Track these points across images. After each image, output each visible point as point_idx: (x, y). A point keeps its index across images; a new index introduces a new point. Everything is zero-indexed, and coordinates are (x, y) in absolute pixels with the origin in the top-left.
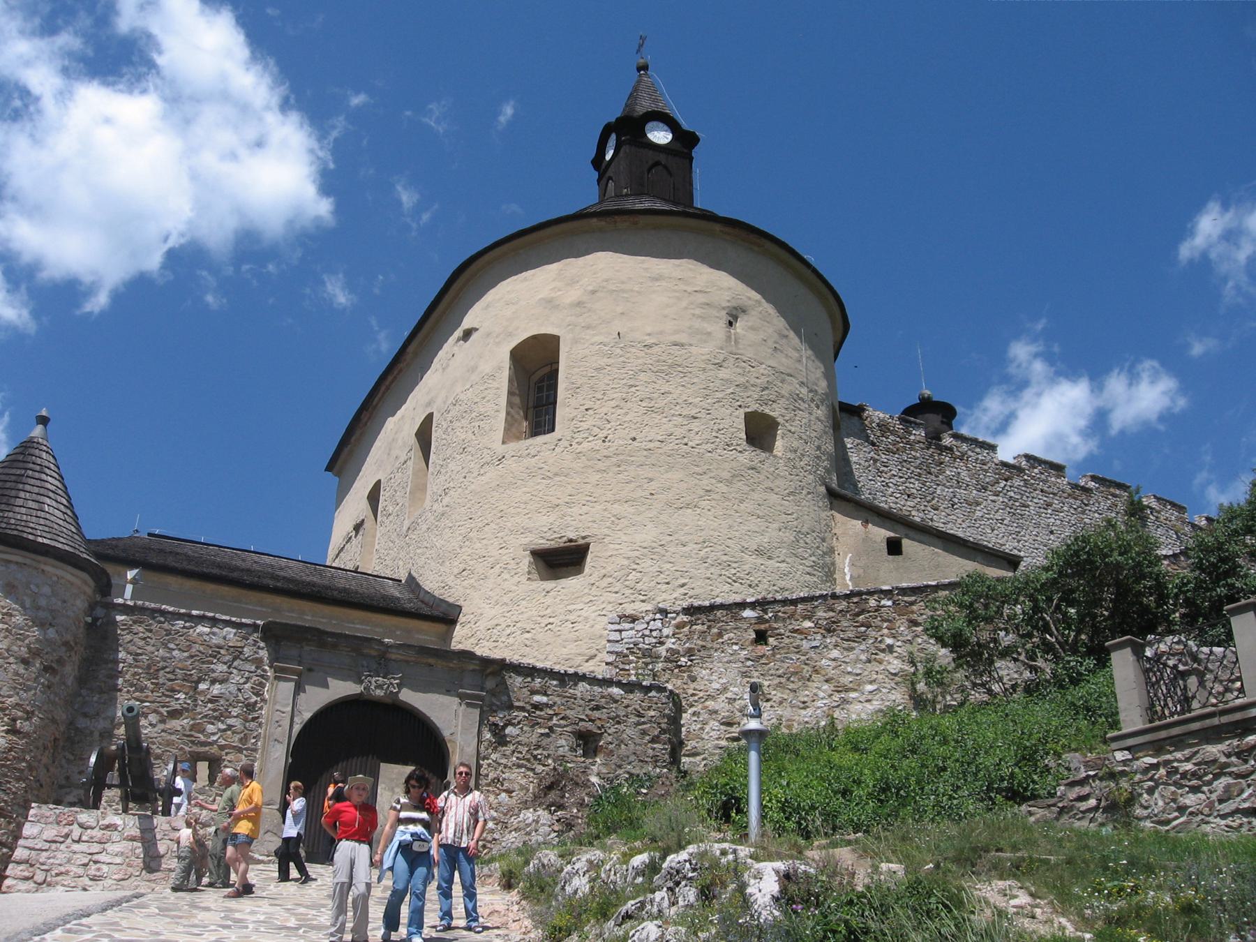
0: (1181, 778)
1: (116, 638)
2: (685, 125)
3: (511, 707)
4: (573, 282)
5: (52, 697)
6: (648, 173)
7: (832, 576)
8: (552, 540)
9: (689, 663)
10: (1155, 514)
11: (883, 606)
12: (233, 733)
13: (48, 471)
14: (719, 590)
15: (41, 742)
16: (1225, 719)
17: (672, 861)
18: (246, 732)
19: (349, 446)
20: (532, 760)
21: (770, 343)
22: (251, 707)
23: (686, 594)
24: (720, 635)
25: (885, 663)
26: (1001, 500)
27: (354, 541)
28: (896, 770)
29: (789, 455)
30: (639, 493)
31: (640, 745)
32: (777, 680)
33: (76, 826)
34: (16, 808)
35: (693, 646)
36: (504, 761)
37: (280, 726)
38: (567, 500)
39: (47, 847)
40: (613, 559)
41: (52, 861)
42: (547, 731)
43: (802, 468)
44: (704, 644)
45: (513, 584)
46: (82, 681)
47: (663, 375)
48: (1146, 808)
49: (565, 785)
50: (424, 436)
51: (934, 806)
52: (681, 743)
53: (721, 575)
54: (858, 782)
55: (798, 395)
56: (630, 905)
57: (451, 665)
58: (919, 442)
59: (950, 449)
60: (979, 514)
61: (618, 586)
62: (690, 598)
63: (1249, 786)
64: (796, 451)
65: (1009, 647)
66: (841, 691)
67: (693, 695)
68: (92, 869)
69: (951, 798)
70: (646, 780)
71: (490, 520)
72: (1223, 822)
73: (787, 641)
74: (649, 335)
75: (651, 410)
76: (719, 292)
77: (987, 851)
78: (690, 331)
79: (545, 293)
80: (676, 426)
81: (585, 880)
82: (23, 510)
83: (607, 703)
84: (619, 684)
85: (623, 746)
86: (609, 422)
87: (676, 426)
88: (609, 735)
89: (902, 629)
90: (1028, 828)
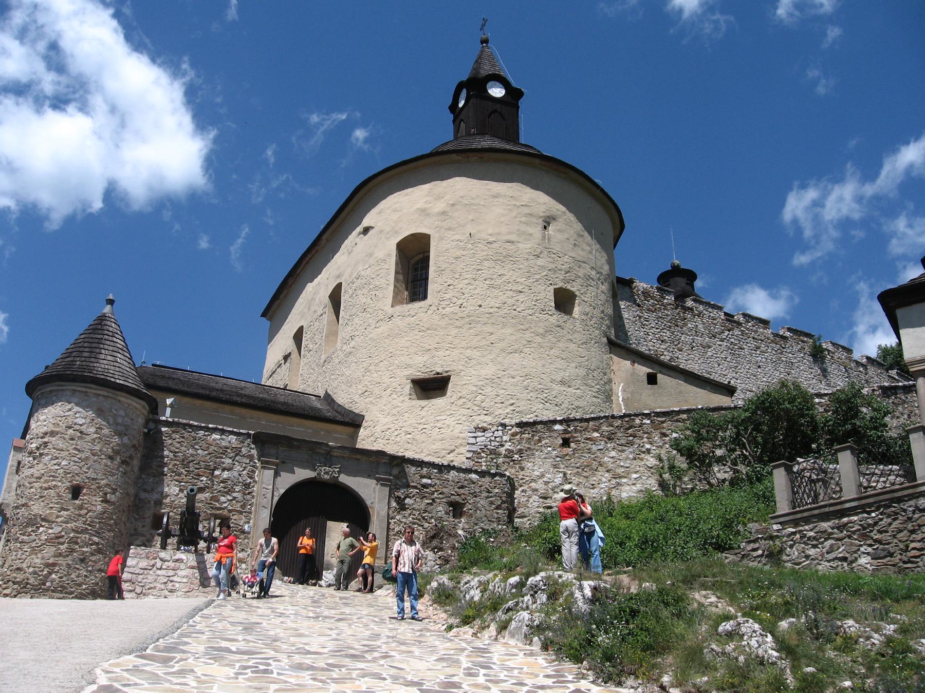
0: (808, 540)
1: (162, 442)
2: (514, 84)
3: (408, 486)
4: (439, 198)
5: (127, 479)
6: (489, 118)
7: (610, 398)
8: (426, 373)
9: (520, 458)
10: (831, 355)
11: (645, 424)
12: (237, 502)
13: (117, 336)
14: (535, 408)
15: (121, 508)
16: (832, 509)
17: (532, 581)
18: (245, 501)
19: (279, 301)
20: (422, 520)
21: (572, 241)
22: (247, 486)
23: (514, 410)
24: (540, 441)
25: (645, 460)
26: (725, 344)
27: (283, 367)
28: (651, 531)
29: (583, 317)
30: (484, 342)
31: (489, 511)
32: (576, 470)
33: (158, 560)
34: (108, 548)
35: (522, 448)
36: (404, 520)
37: (265, 498)
38: (435, 347)
39: (142, 572)
40: (466, 386)
41: (145, 580)
42: (431, 501)
43: (592, 326)
44: (529, 446)
45: (400, 402)
46: (142, 469)
47: (499, 263)
48: (788, 556)
49: (443, 536)
50: (335, 298)
51: (673, 553)
52: (514, 510)
53: (537, 398)
54: (629, 538)
55: (589, 276)
56: (511, 603)
57: (371, 460)
58: (670, 304)
59: (691, 309)
60: (710, 354)
61: (469, 405)
62: (517, 413)
63: (843, 545)
64: (587, 314)
65: (721, 457)
66: (616, 478)
67: (522, 479)
68: (170, 586)
69: (683, 548)
70: (493, 533)
71: (383, 358)
72: (828, 564)
73: (582, 445)
74: (491, 235)
75: (491, 286)
76: (538, 206)
77: (699, 577)
78: (518, 233)
79: (420, 205)
80: (508, 297)
81: (478, 591)
82: (105, 362)
83: (468, 484)
84: (476, 472)
85: (478, 511)
86: (464, 294)
87: (508, 297)
88: (470, 504)
89: (656, 438)
90: (722, 565)
